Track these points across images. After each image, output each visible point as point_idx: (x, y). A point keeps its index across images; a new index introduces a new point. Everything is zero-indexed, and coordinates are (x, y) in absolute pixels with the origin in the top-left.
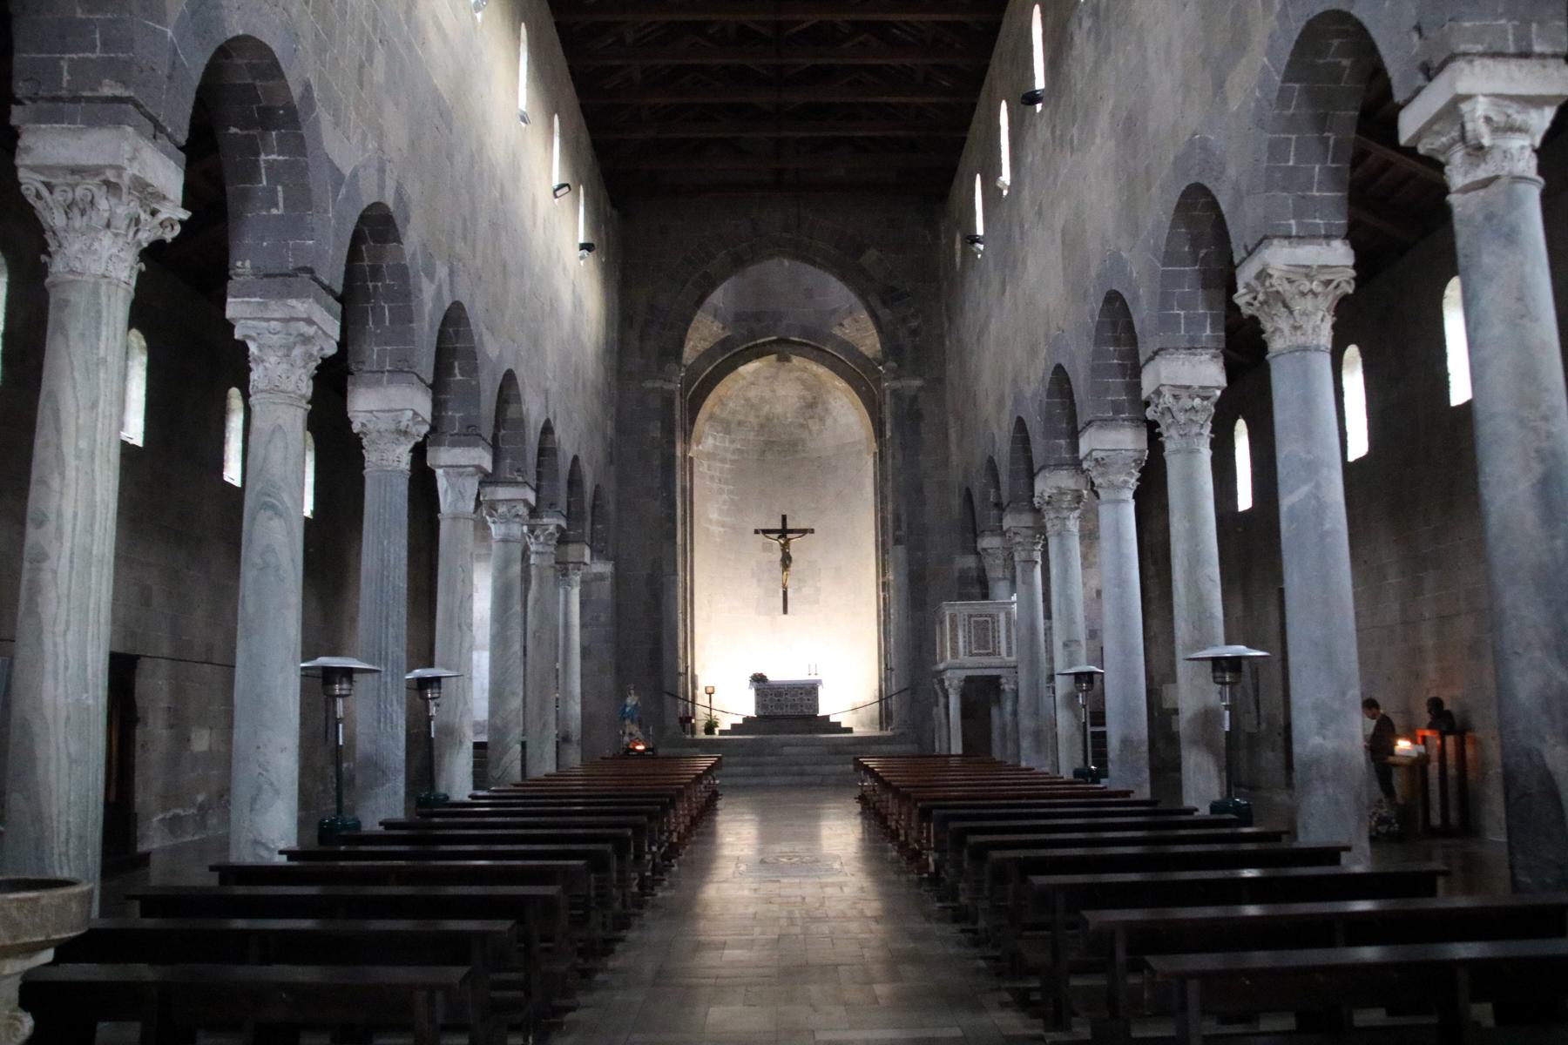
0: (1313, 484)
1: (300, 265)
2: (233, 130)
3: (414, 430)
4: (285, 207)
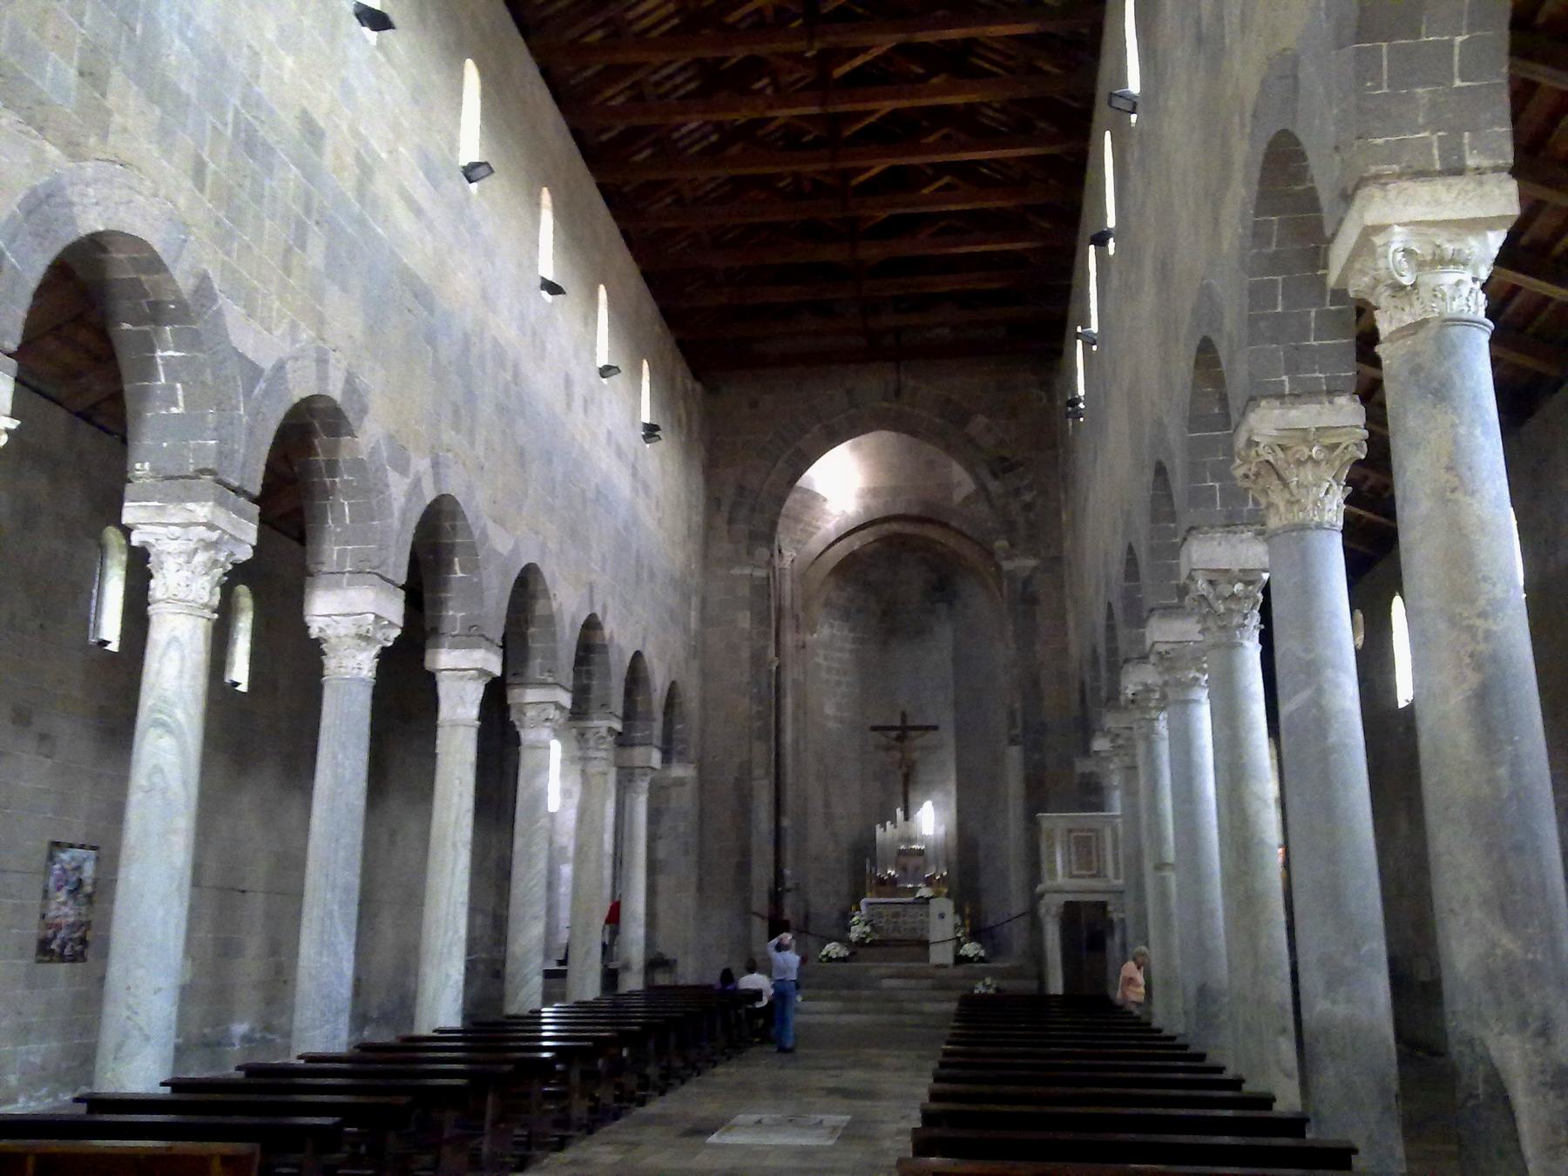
0: (1314, 687)
1: (201, 466)
2: (126, 326)
3: (379, 636)
4: (186, 406)
